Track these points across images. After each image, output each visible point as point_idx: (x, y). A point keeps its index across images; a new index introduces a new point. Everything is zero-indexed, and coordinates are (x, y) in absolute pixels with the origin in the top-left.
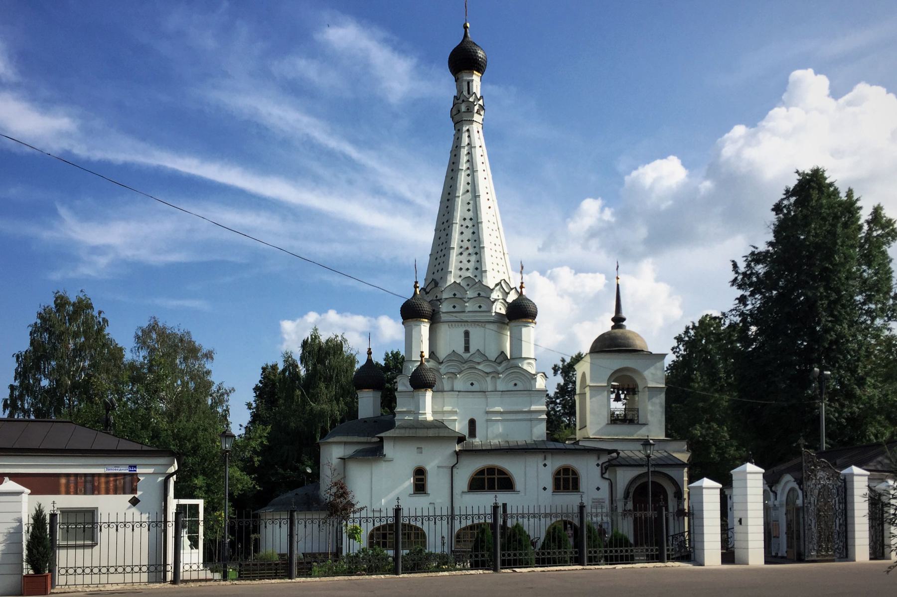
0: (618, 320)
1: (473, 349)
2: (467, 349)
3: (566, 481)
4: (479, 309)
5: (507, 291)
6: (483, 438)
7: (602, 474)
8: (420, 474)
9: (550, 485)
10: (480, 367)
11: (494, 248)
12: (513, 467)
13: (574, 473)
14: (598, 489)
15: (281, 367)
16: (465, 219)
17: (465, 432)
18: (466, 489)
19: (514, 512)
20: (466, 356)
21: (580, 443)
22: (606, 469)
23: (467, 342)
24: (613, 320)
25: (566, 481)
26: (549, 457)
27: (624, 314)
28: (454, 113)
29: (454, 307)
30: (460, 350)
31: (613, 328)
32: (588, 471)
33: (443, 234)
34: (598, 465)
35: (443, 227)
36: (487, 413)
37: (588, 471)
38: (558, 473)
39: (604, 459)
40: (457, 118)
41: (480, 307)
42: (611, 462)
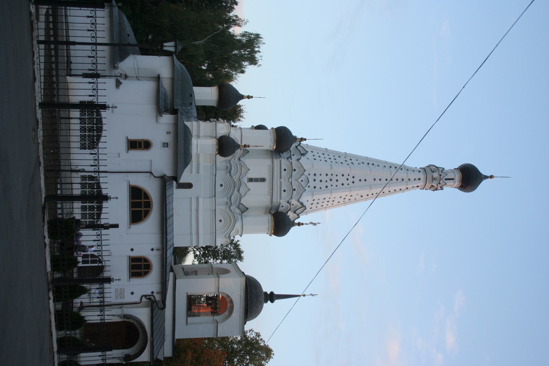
0: (272, 297)
1: (251, 185)
2: (251, 180)
3: (139, 267)
4: (282, 190)
5: (297, 212)
6: (178, 196)
7: (145, 296)
8: (146, 145)
9: (134, 254)
10: (236, 191)
11: (331, 200)
12: (151, 222)
13: (146, 274)
14: (132, 293)
15: (236, 31)
16: (353, 177)
17: (183, 180)
18: (131, 184)
19: (104, 237)
20: (245, 180)
21: (171, 274)
22: (150, 299)
23: (256, 180)
24: (272, 293)
25: (139, 267)
26: (159, 253)
27: (277, 301)
28: (433, 168)
29: (285, 170)
30: (250, 175)
31: (266, 293)
32: (148, 284)
33: (342, 159)
34: (153, 293)
35: (348, 159)
36: (198, 198)
37: (148, 284)
38: (146, 260)
39: (158, 297)
40: (428, 170)
41: (285, 191)
42: (156, 305)
